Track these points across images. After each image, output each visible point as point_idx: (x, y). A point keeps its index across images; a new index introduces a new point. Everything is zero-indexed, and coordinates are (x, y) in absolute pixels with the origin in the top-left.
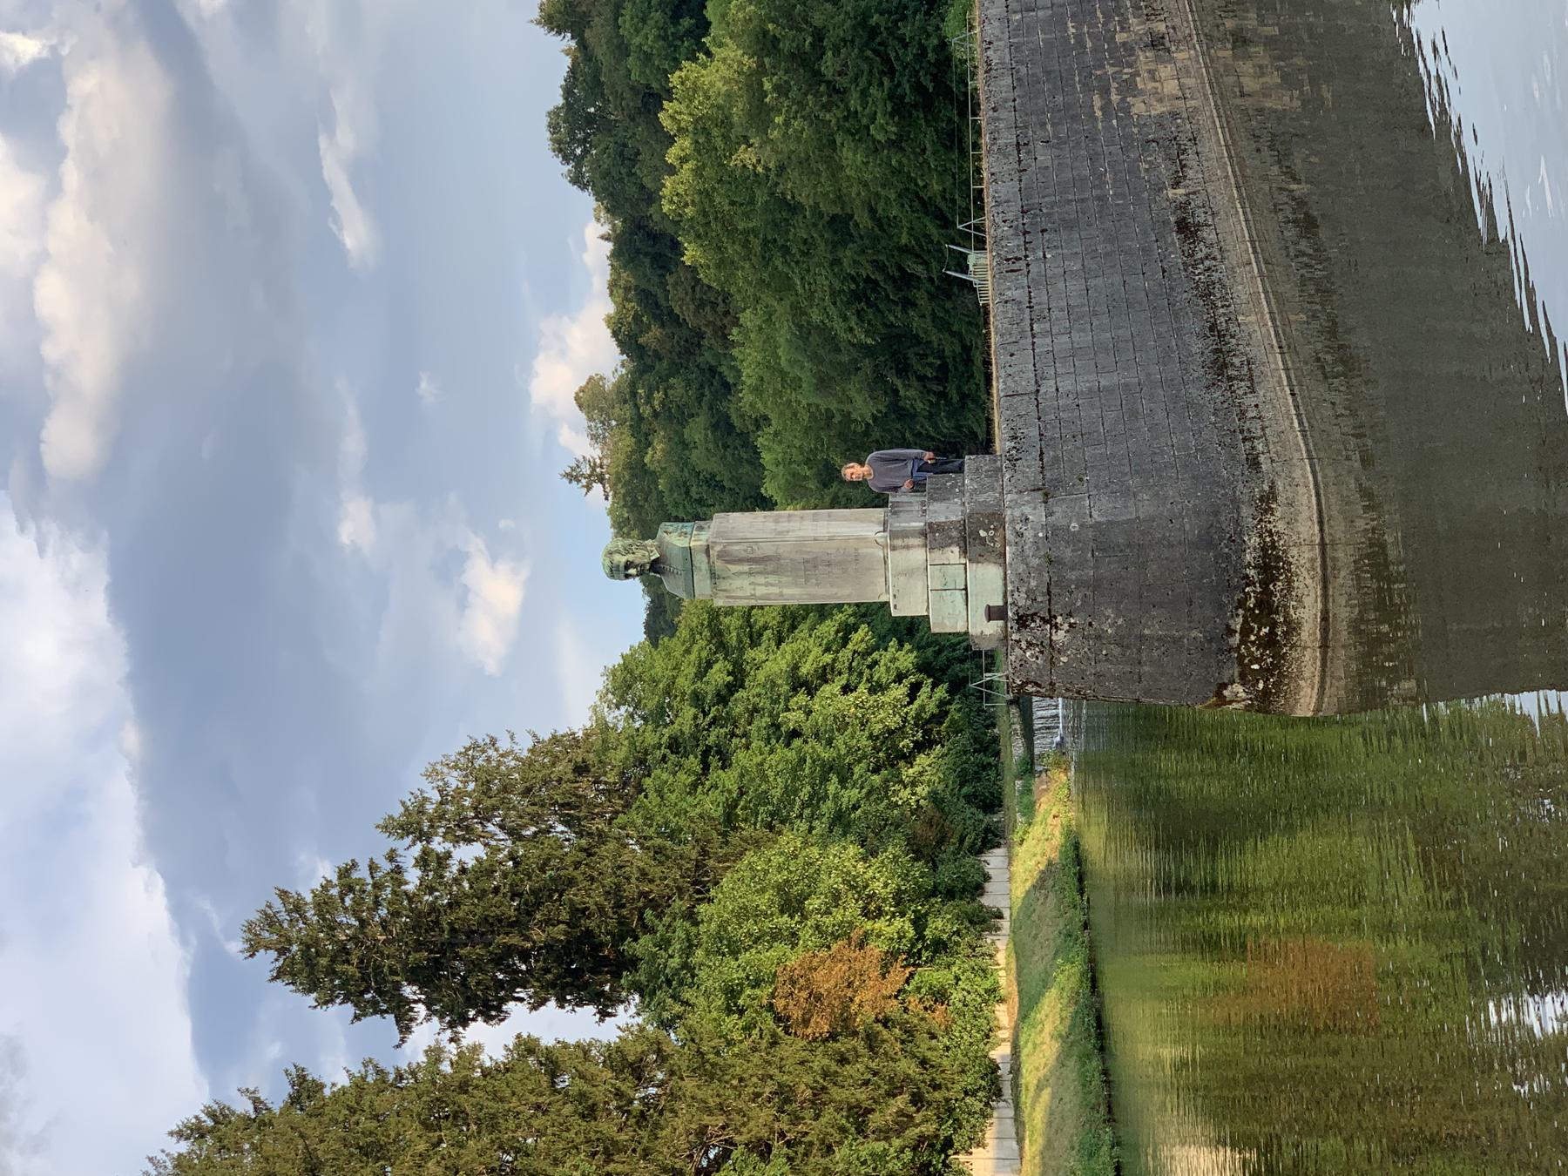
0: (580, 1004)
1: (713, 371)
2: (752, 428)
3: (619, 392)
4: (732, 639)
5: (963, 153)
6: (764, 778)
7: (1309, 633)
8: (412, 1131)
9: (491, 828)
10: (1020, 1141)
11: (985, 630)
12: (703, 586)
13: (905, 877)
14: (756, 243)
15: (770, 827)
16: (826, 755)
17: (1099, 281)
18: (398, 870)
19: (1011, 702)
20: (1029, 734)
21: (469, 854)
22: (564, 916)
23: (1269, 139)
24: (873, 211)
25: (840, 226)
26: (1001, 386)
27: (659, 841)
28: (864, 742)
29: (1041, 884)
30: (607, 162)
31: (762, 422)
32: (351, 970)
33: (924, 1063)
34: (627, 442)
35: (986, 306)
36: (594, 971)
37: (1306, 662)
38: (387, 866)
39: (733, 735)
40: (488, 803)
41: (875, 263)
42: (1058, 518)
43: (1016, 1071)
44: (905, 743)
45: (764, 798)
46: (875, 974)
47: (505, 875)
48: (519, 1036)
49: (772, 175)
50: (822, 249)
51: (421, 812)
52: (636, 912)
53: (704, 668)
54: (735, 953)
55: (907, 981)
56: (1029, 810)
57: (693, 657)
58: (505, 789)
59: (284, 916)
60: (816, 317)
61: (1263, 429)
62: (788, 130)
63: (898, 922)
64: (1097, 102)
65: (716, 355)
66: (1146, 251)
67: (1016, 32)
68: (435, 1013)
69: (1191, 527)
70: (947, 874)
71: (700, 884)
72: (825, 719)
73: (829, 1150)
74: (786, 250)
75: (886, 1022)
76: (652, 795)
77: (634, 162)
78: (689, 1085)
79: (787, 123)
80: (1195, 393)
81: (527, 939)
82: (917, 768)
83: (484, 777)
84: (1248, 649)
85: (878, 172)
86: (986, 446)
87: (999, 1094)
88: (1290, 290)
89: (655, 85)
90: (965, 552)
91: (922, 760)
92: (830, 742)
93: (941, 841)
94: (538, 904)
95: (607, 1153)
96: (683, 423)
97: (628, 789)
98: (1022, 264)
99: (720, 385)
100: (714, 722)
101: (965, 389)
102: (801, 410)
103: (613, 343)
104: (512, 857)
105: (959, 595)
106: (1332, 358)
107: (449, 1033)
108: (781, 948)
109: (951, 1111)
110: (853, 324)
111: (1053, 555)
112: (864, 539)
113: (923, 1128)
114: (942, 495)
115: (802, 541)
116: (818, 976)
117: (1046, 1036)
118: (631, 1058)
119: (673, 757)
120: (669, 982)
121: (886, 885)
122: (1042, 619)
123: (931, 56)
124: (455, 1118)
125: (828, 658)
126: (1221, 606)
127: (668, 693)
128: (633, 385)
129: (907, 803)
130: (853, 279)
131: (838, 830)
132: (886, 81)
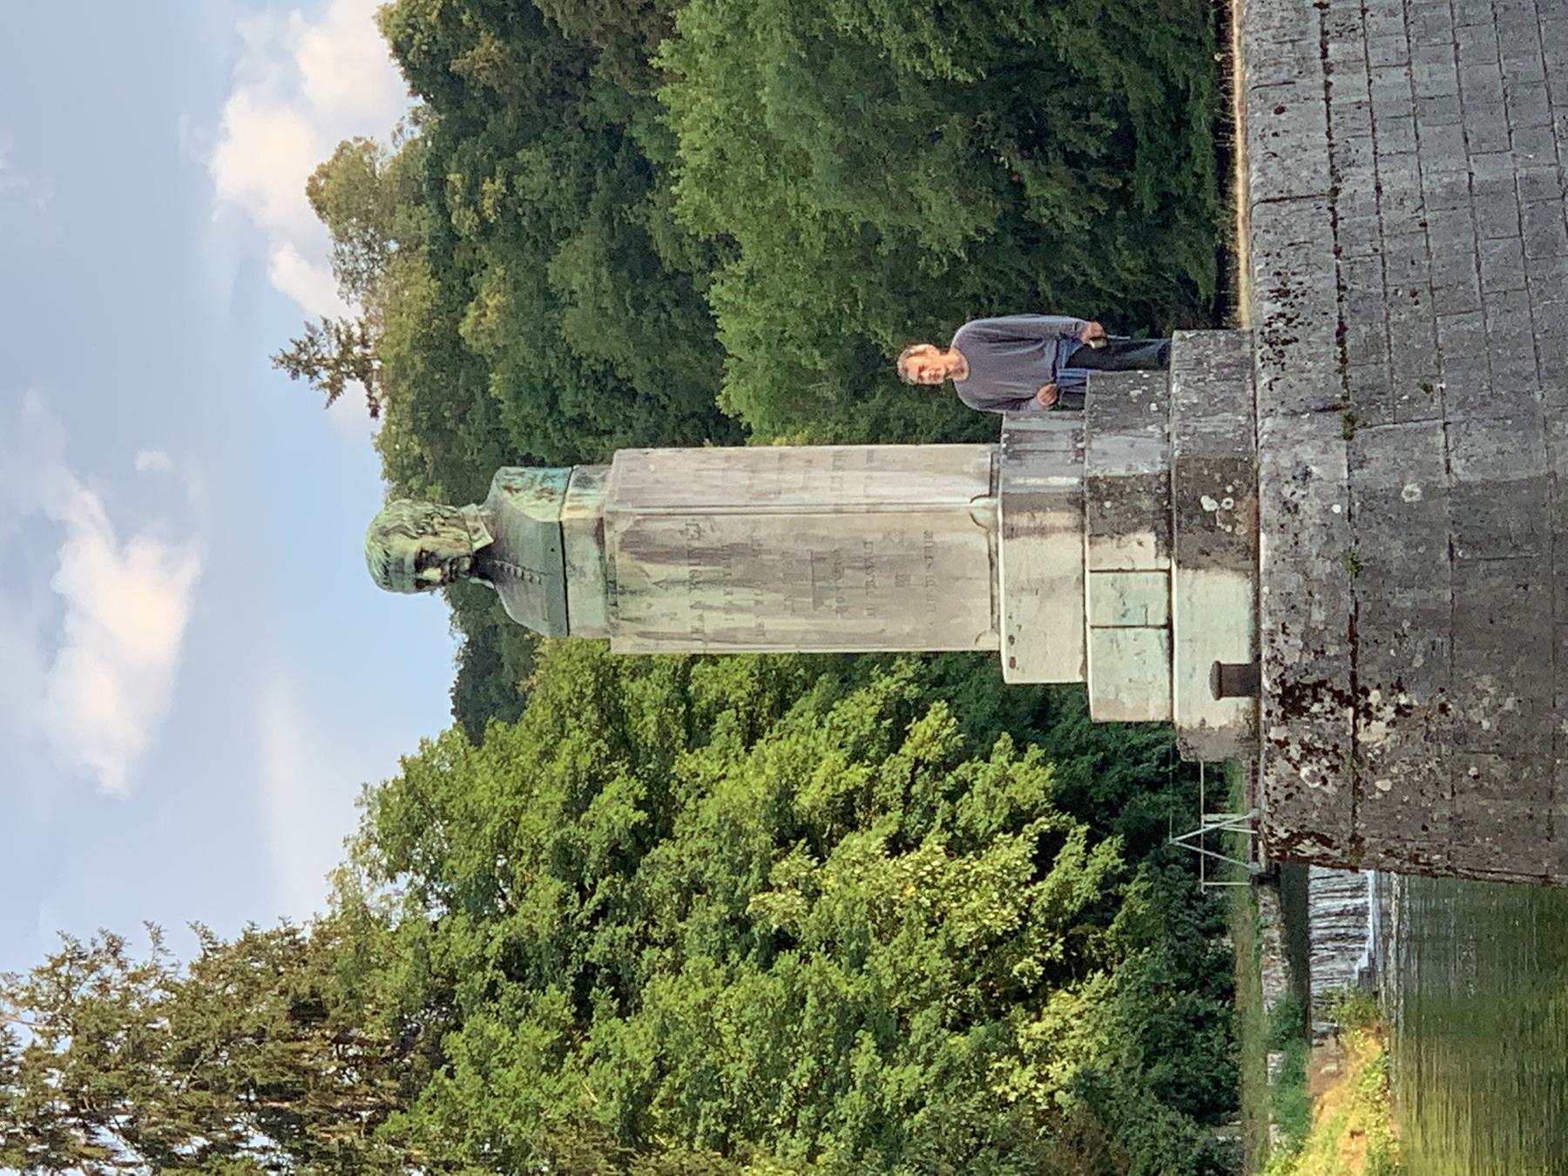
1: (614, 135)
2: (698, 263)
3: (405, 179)
4: (647, 729)
6: (713, 1038)
9: (105, 1136)
11: (1211, 717)
15: (723, 1145)
16: (851, 988)
19: (1260, 880)
26: (1255, 179)
31: (720, 251)
34: (423, 288)
39: (646, 941)
40: (102, 1081)
44: (1026, 966)
45: (710, 1083)
53: (579, 801)
56: (1298, 1120)
57: (559, 767)
58: (139, 1052)
76: (464, 1070)
82: (1049, 1022)
83: (93, 1024)
90: (1169, 544)
91: (1061, 1004)
92: (859, 960)
97: (411, 1058)
99: (627, 166)
100: (602, 913)
101: (1172, 187)
102: (804, 222)
103: (395, 69)
105: (1154, 641)
110: (925, 37)
111: (1364, 552)
114: (1121, 416)
119: (511, 989)
122: (1337, 694)
127: (502, 844)
128: (436, 164)
129: (1026, 1098)
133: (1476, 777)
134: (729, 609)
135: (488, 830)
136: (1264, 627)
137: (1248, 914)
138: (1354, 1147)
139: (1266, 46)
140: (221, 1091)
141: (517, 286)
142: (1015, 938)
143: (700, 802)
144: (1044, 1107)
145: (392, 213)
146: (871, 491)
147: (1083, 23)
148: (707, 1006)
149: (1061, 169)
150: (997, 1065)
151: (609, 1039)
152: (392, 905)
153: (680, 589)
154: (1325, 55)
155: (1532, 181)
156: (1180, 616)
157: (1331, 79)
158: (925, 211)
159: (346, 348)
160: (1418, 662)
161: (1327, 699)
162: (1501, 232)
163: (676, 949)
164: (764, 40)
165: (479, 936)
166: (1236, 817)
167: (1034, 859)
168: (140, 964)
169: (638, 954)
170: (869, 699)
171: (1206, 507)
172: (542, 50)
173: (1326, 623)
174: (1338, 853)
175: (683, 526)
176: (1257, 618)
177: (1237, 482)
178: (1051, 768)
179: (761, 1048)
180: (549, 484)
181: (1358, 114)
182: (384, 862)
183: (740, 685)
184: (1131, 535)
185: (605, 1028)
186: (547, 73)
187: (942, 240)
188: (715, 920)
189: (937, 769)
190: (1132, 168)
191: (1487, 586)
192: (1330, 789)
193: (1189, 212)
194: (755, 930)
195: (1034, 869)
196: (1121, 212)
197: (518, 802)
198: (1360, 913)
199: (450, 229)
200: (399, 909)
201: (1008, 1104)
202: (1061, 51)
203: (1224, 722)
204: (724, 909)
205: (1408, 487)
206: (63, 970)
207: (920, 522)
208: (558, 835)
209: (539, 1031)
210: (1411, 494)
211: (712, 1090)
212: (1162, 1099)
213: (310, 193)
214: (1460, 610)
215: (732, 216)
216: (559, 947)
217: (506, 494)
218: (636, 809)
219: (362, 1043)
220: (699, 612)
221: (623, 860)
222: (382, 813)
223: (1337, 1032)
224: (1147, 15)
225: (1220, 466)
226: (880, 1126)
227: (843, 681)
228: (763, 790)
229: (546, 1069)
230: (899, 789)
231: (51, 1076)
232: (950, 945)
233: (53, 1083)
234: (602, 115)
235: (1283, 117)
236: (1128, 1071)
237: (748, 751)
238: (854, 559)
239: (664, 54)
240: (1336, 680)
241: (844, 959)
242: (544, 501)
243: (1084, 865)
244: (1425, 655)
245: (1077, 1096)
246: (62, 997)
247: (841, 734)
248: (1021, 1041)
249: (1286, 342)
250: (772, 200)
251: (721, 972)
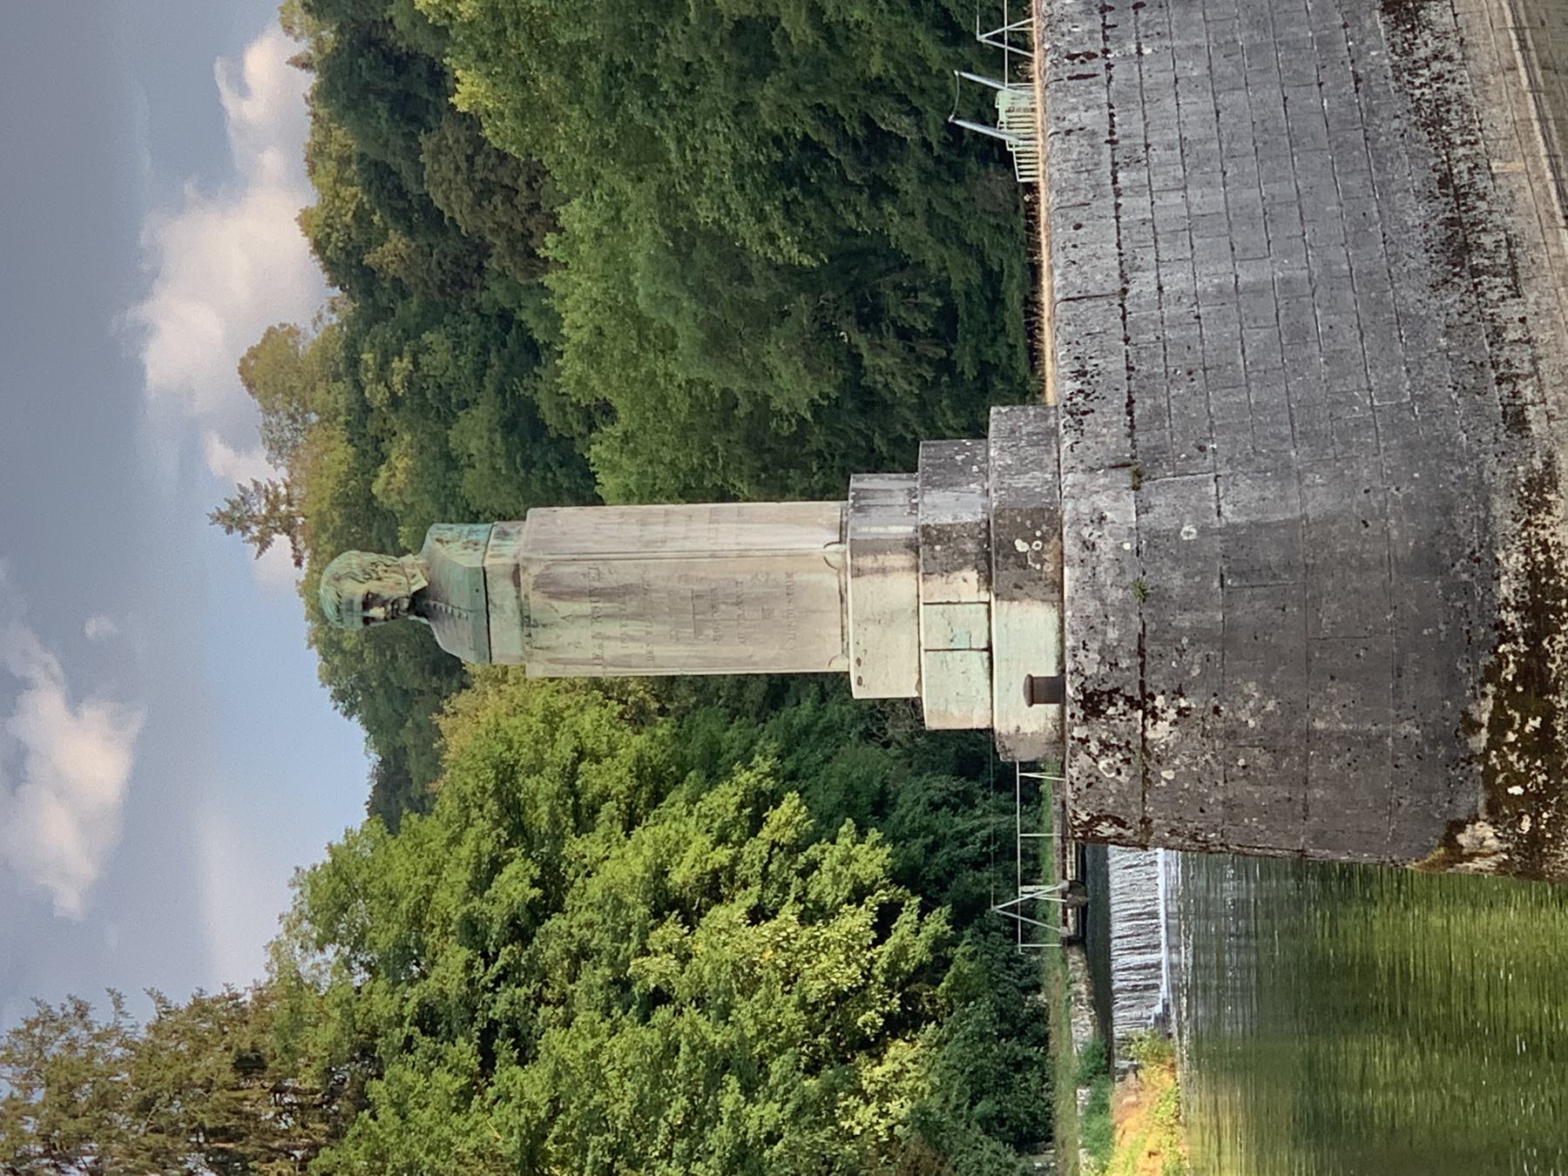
1: (506, 318)
2: (579, 428)
3: (325, 359)
4: (540, 817)
6: (599, 1081)
11: (1024, 724)
12: (507, 641)
14: (592, 71)
16: (719, 1037)
17: (1239, 96)
19: (1069, 942)
26: (1058, 282)
28: (790, 1014)
31: (598, 417)
34: (341, 454)
35: (1031, 188)
39: (540, 1000)
40: (70, 1126)
42: (1161, 515)
45: (597, 1120)
50: (718, 88)
53: (486, 874)
56: (1102, 1142)
57: (464, 852)
58: (104, 1101)
60: (705, 212)
61: (1534, 362)
65: (512, 289)
66: (1325, 43)
69: (1402, 535)
72: (716, 971)
74: (649, 85)
76: (386, 1113)
80: (1412, 296)
82: (889, 1066)
83: (63, 1077)
84: (1502, 757)
86: (1027, 391)
90: (989, 580)
91: (899, 1051)
92: (724, 1013)
96: (447, 418)
97: (339, 1102)
98: (1098, 65)
99: (517, 345)
101: (989, 355)
102: (672, 390)
103: (315, 266)
105: (978, 661)
110: (775, 227)
111: (1149, 581)
112: (806, 555)
114: (948, 476)
119: (425, 1042)
122: (1128, 699)
127: (416, 920)
128: (352, 346)
130: (777, 141)
133: (1244, 767)
134: (625, 638)
135: (404, 905)
136: (1068, 644)
137: (1059, 973)
138: (1151, 1166)
139: (1066, 175)
140: (175, 1133)
141: (422, 449)
142: (859, 993)
143: (588, 881)
144: (885, 1139)
145: (313, 389)
146: (741, 539)
147: (912, 214)
148: (594, 1054)
149: (892, 341)
150: (843, 1104)
151: (510, 1084)
152: (321, 973)
153: (583, 622)
154: (1115, 182)
155: (1287, 282)
156: (998, 638)
157: (1120, 201)
158: (777, 379)
159: (274, 507)
160: (1196, 672)
161: (1121, 703)
162: (1262, 323)
163: (567, 1007)
164: (636, 231)
165: (397, 998)
166: (1048, 888)
167: (874, 927)
168: (103, 1025)
169: (535, 1011)
170: (731, 791)
171: (1020, 549)
172: (442, 245)
173: (1120, 641)
174: (1129, 833)
175: (586, 570)
176: (1062, 641)
177: (1044, 528)
178: (889, 848)
179: (641, 1090)
180: (474, 537)
181: (1144, 229)
182: (315, 935)
183: (620, 780)
184: (957, 574)
185: (506, 1074)
186: (447, 265)
187: (790, 403)
188: (600, 982)
189: (790, 852)
190: (954, 340)
191: (1252, 609)
192: (1123, 778)
193: (1003, 378)
194: (635, 989)
195: (874, 935)
196: (945, 378)
197: (430, 881)
198: (1157, 966)
199: (364, 401)
200: (328, 976)
201: (854, 1137)
202: (892, 239)
203: (1035, 728)
204: (608, 972)
205: (1186, 528)
206: (37, 1031)
208: (464, 909)
209: (449, 1077)
210: (1188, 533)
211: (599, 1127)
212: (987, 1132)
213: (241, 373)
214: (1230, 627)
215: (610, 386)
216: (466, 1005)
217: (438, 545)
218: (532, 887)
219: (296, 1092)
220: (597, 642)
222: (313, 891)
223: (1136, 1068)
224: (968, 208)
225: (1030, 515)
226: (745, 1156)
227: (709, 777)
228: (641, 868)
229: (456, 1110)
230: (758, 868)
231: (28, 1122)
232: (803, 999)
233: (29, 1128)
234: (496, 302)
235: (1081, 232)
236: (958, 1107)
237: (628, 836)
238: (728, 596)
239: (549, 246)
240: (1128, 688)
241: (712, 1013)
242: (470, 551)
243: (918, 932)
244: (1201, 665)
245: (913, 1129)
246: (36, 1055)
247: (708, 821)
248: (865, 1083)
249: (1085, 413)
250: (643, 370)
251: (606, 1026)
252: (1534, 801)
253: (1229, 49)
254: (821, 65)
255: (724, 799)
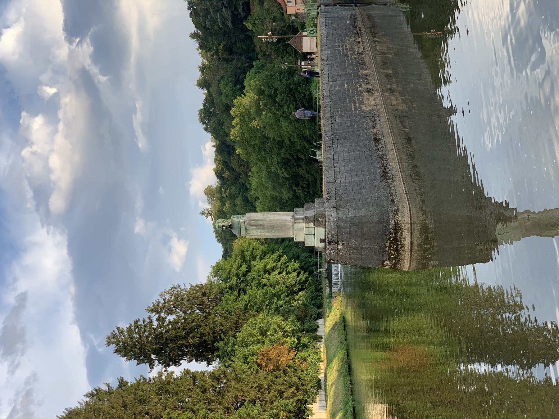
0: (202, 361)
1: (243, 184)
4: (248, 258)
5: (316, 124)
6: (256, 298)
7: (407, 247)
8: (153, 396)
9: (178, 310)
10: (326, 401)
11: (320, 246)
12: (243, 232)
13: (295, 326)
14: (257, 148)
15: (257, 311)
18: (151, 322)
19: (326, 278)
20: (331, 287)
21: (172, 318)
22: (198, 336)
23: (399, 118)
24: (290, 140)
25: (281, 144)
27: (225, 315)
29: (333, 328)
30: (215, 125)
32: (137, 350)
33: (299, 378)
34: (219, 204)
36: (206, 352)
37: (406, 255)
38: (148, 321)
39: (247, 285)
40: (177, 303)
41: (290, 154)
43: (325, 381)
44: (296, 289)
45: (255, 303)
46: (286, 353)
47: (182, 324)
48: (185, 369)
49: (262, 129)
50: (275, 151)
51: (158, 306)
52: (218, 335)
53: (239, 267)
54: (246, 347)
55: (295, 356)
56: (330, 308)
58: (182, 299)
59: (118, 334)
60: (273, 169)
62: (266, 116)
63: (293, 339)
64: (353, 106)
66: (365, 145)
67: (331, 87)
68: (160, 363)
69: (376, 218)
70: (307, 326)
71: (237, 327)
73: (272, 403)
74: (265, 150)
75: (289, 367)
76: (224, 302)
77: (222, 125)
78: (233, 383)
79: (266, 114)
81: (188, 342)
83: (176, 296)
85: (292, 128)
86: (321, 196)
87: (321, 388)
88: (404, 157)
89: (229, 104)
92: (275, 288)
93: (306, 316)
94: (191, 332)
95: (209, 402)
96: (234, 199)
97: (217, 300)
98: (332, 148)
99: (245, 188)
100: (242, 282)
104: (184, 318)
105: (313, 236)
106: (414, 174)
107: (164, 369)
108: (260, 345)
109: (307, 392)
113: (299, 397)
114: (309, 209)
115: (270, 220)
116: (270, 353)
117: (334, 371)
118: (217, 376)
119: (230, 291)
120: (228, 355)
121: (290, 328)
123: (307, 97)
124: (166, 392)
125: (275, 264)
126: (383, 239)
127: (229, 273)
128: (220, 188)
131: (276, 312)
132: (294, 103)
207: (284, 221)
214: (350, 231)
221: (245, 275)
252: (395, 258)
253: (351, 146)
254: (290, 148)
255: (275, 256)
